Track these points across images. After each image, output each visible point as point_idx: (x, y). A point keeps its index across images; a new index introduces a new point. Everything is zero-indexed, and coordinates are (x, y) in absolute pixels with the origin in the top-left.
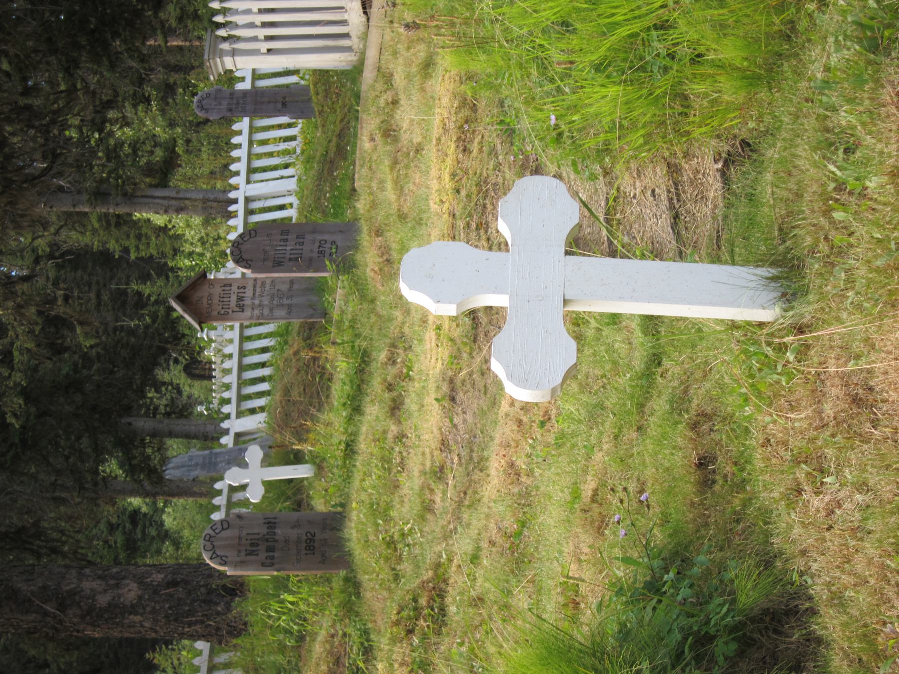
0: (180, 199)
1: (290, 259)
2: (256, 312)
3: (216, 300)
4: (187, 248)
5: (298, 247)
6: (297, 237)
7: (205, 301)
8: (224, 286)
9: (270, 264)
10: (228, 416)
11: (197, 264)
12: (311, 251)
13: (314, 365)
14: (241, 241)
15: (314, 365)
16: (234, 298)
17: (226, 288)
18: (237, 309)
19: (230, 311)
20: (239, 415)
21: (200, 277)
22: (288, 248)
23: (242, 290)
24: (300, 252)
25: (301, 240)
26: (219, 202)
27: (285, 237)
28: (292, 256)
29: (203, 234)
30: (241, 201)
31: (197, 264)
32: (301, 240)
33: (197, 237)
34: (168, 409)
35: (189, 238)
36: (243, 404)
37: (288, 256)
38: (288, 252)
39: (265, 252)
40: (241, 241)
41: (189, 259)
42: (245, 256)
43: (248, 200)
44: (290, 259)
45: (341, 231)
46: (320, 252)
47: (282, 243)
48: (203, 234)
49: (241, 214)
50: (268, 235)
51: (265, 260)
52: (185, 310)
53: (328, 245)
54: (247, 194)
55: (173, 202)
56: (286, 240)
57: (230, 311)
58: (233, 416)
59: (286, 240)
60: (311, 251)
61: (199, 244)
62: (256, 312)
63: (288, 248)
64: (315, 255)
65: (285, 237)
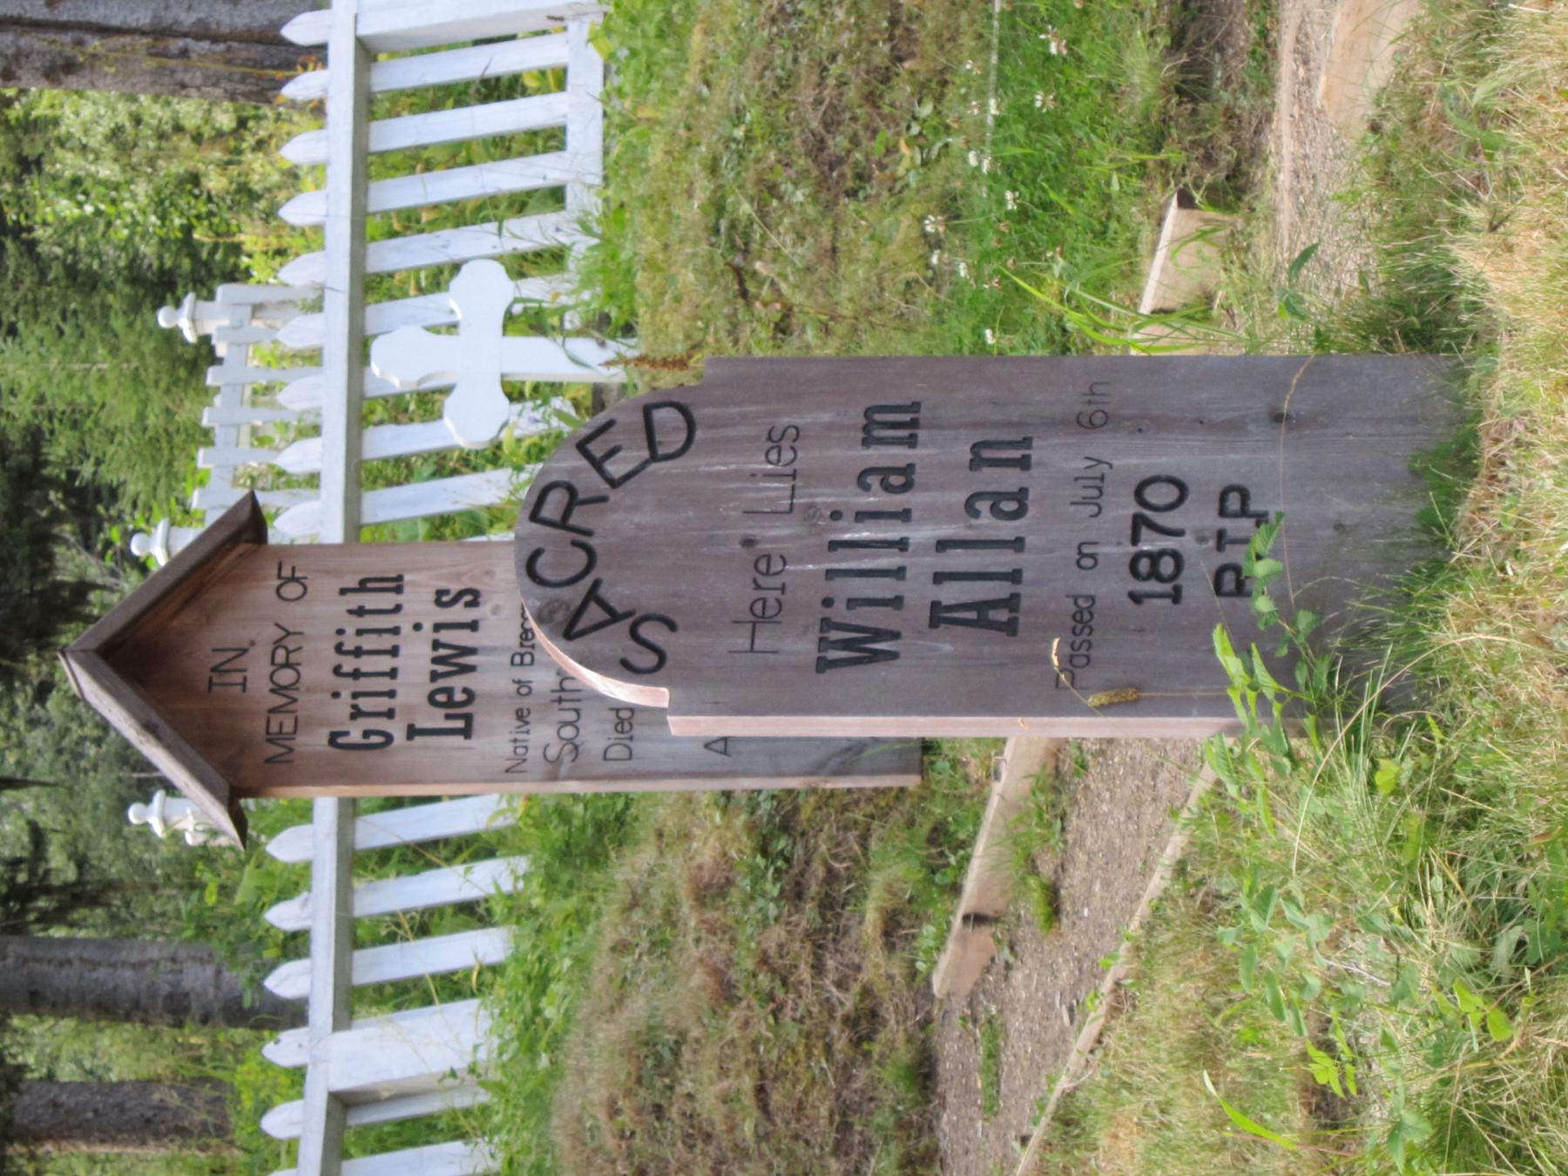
0: (64, 27)
1: (939, 615)
2: (543, 735)
3: (317, 667)
4: (68, 163)
5: (987, 525)
6: (976, 463)
7: (258, 671)
8: (363, 587)
9: (805, 647)
10: (293, 1014)
11: (98, 213)
12: (1085, 558)
13: (818, 968)
14: (589, 482)
15: (818, 968)
16: (416, 657)
17: (371, 601)
18: (436, 720)
19: (397, 729)
20: (345, 1013)
21: (234, 539)
22: (921, 534)
23: (459, 613)
24: (1003, 560)
25: (1009, 479)
26: (215, 39)
27: (897, 455)
28: (951, 593)
29: (123, 118)
30: (342, 56)
31: (98, 213)
32: (1009, 479)
33: (103, 129)
34: (22, 878)
35: (77, 132)
36: (361, 957)
37: (919, 592)
38: (921, 565)
39: (763, 563)
40: (589, 482)
41: (71, 197)
42: (618, 592)
43: (367, 52)
44: (939, 615)
45: (1277, 418)
46: (1145, 567)
47: (875, 499)
48: (123, 118)
49: (341, 109)
50: (775, 441)
51: (760, 617)
52: (149, 728)
53: (1198, 517)
54: (365, 30)
55: (35, 42)
56: (905, 478)
57: (397, 729)
58: (322, 1010)
59: (905, 478)
60: (1085, 558)
61: (108, 150)
62: (543, 735)
63: (921, 534)
64: (1111, 586)
65: (897, 455)
